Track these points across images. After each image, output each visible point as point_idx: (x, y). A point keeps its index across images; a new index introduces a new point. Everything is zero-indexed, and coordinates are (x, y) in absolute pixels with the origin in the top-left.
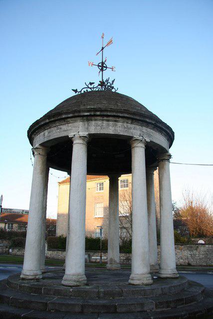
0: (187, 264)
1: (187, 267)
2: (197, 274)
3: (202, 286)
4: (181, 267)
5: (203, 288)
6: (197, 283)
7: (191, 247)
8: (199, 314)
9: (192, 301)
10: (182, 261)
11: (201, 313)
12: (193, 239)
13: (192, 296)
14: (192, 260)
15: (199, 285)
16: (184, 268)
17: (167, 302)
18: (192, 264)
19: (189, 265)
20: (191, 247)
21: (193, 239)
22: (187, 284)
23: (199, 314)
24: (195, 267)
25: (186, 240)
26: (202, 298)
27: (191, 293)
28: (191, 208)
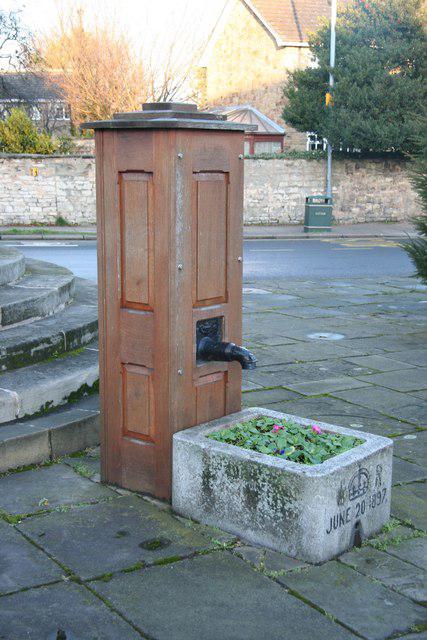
0: (53, 220)
1: (53, 229)
2: (81, 248)
3: (68, 273)
4: (33, 229)
5: (68, 280)
6: (57, 267)
7: (69, 167)
8: (41, 347)
9: (26, 316)
10: (39, 210)
11: (47, 346)
12: (80, 143)
13: (26, 303)
14: (71, 208)
15: (59, 271)
16: (40, 233)
17: (332, 455)
18: (71, 220)
19: (61, 222)
20: (69, 167)
21: (80, 143)
22: (17, 270)
23: (41, 347)
24: (78, 230)
25: (55, 142)
26: (63, 306)
27: (28, 293)
28: (80, 34)
